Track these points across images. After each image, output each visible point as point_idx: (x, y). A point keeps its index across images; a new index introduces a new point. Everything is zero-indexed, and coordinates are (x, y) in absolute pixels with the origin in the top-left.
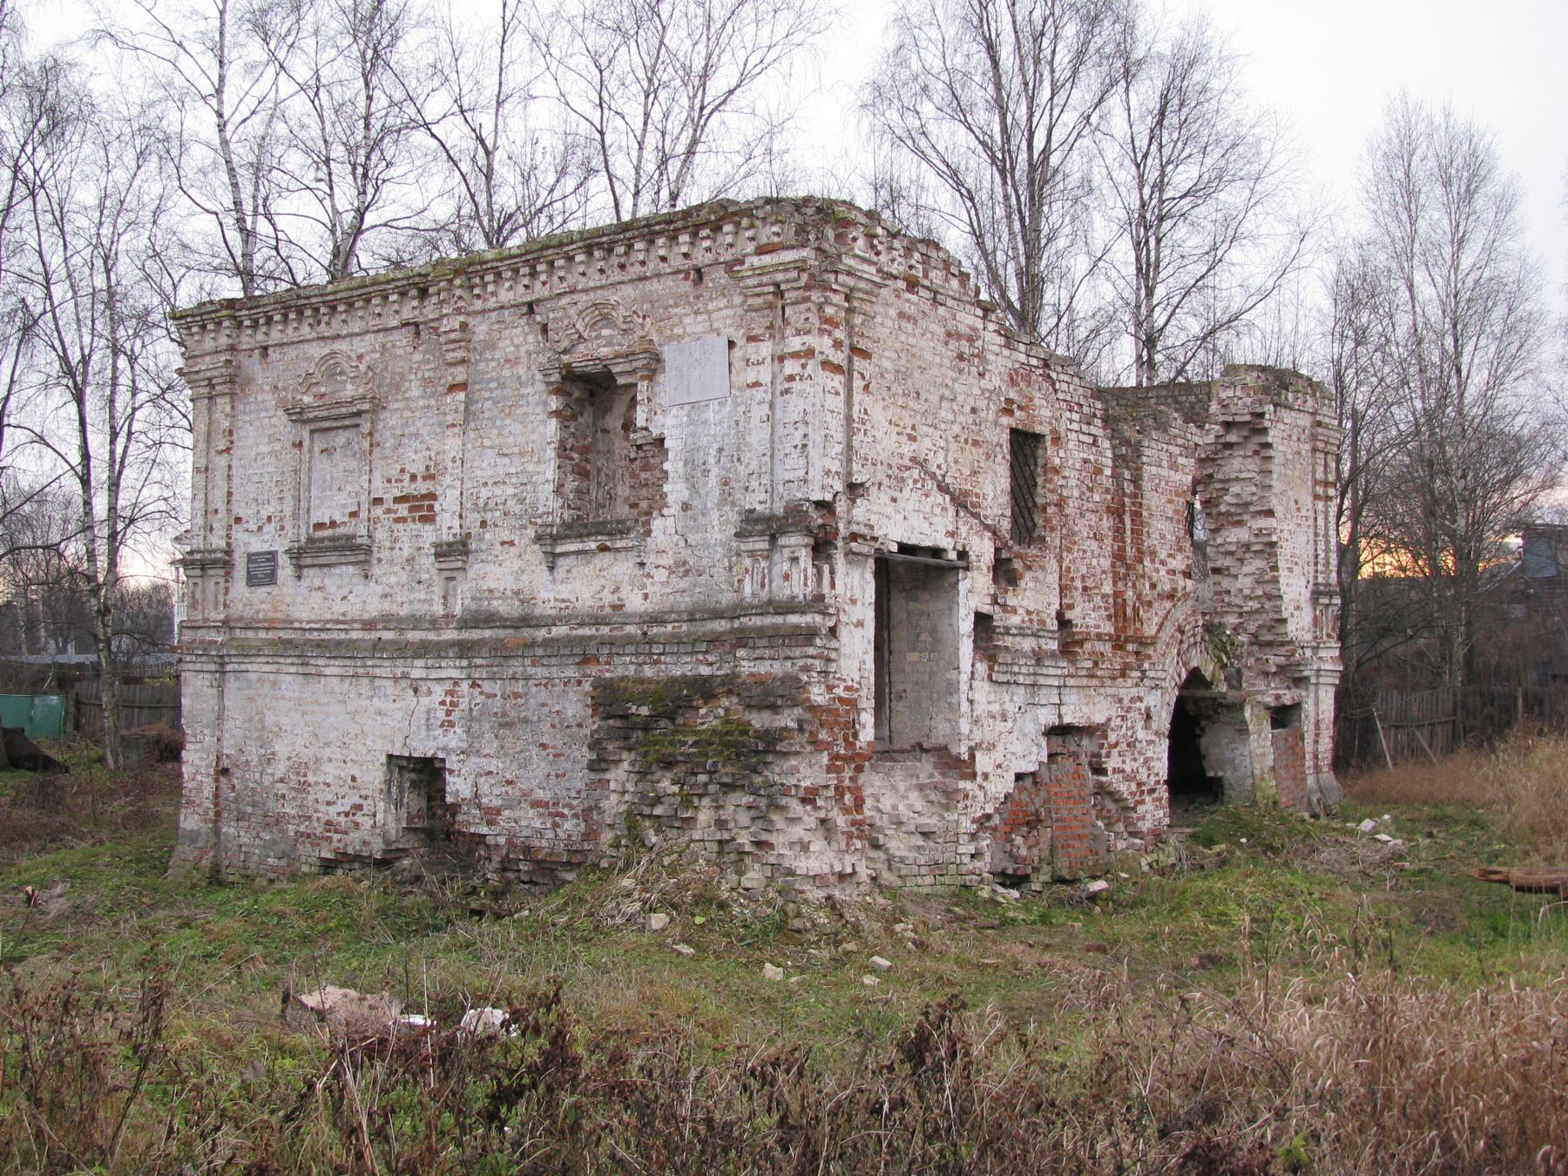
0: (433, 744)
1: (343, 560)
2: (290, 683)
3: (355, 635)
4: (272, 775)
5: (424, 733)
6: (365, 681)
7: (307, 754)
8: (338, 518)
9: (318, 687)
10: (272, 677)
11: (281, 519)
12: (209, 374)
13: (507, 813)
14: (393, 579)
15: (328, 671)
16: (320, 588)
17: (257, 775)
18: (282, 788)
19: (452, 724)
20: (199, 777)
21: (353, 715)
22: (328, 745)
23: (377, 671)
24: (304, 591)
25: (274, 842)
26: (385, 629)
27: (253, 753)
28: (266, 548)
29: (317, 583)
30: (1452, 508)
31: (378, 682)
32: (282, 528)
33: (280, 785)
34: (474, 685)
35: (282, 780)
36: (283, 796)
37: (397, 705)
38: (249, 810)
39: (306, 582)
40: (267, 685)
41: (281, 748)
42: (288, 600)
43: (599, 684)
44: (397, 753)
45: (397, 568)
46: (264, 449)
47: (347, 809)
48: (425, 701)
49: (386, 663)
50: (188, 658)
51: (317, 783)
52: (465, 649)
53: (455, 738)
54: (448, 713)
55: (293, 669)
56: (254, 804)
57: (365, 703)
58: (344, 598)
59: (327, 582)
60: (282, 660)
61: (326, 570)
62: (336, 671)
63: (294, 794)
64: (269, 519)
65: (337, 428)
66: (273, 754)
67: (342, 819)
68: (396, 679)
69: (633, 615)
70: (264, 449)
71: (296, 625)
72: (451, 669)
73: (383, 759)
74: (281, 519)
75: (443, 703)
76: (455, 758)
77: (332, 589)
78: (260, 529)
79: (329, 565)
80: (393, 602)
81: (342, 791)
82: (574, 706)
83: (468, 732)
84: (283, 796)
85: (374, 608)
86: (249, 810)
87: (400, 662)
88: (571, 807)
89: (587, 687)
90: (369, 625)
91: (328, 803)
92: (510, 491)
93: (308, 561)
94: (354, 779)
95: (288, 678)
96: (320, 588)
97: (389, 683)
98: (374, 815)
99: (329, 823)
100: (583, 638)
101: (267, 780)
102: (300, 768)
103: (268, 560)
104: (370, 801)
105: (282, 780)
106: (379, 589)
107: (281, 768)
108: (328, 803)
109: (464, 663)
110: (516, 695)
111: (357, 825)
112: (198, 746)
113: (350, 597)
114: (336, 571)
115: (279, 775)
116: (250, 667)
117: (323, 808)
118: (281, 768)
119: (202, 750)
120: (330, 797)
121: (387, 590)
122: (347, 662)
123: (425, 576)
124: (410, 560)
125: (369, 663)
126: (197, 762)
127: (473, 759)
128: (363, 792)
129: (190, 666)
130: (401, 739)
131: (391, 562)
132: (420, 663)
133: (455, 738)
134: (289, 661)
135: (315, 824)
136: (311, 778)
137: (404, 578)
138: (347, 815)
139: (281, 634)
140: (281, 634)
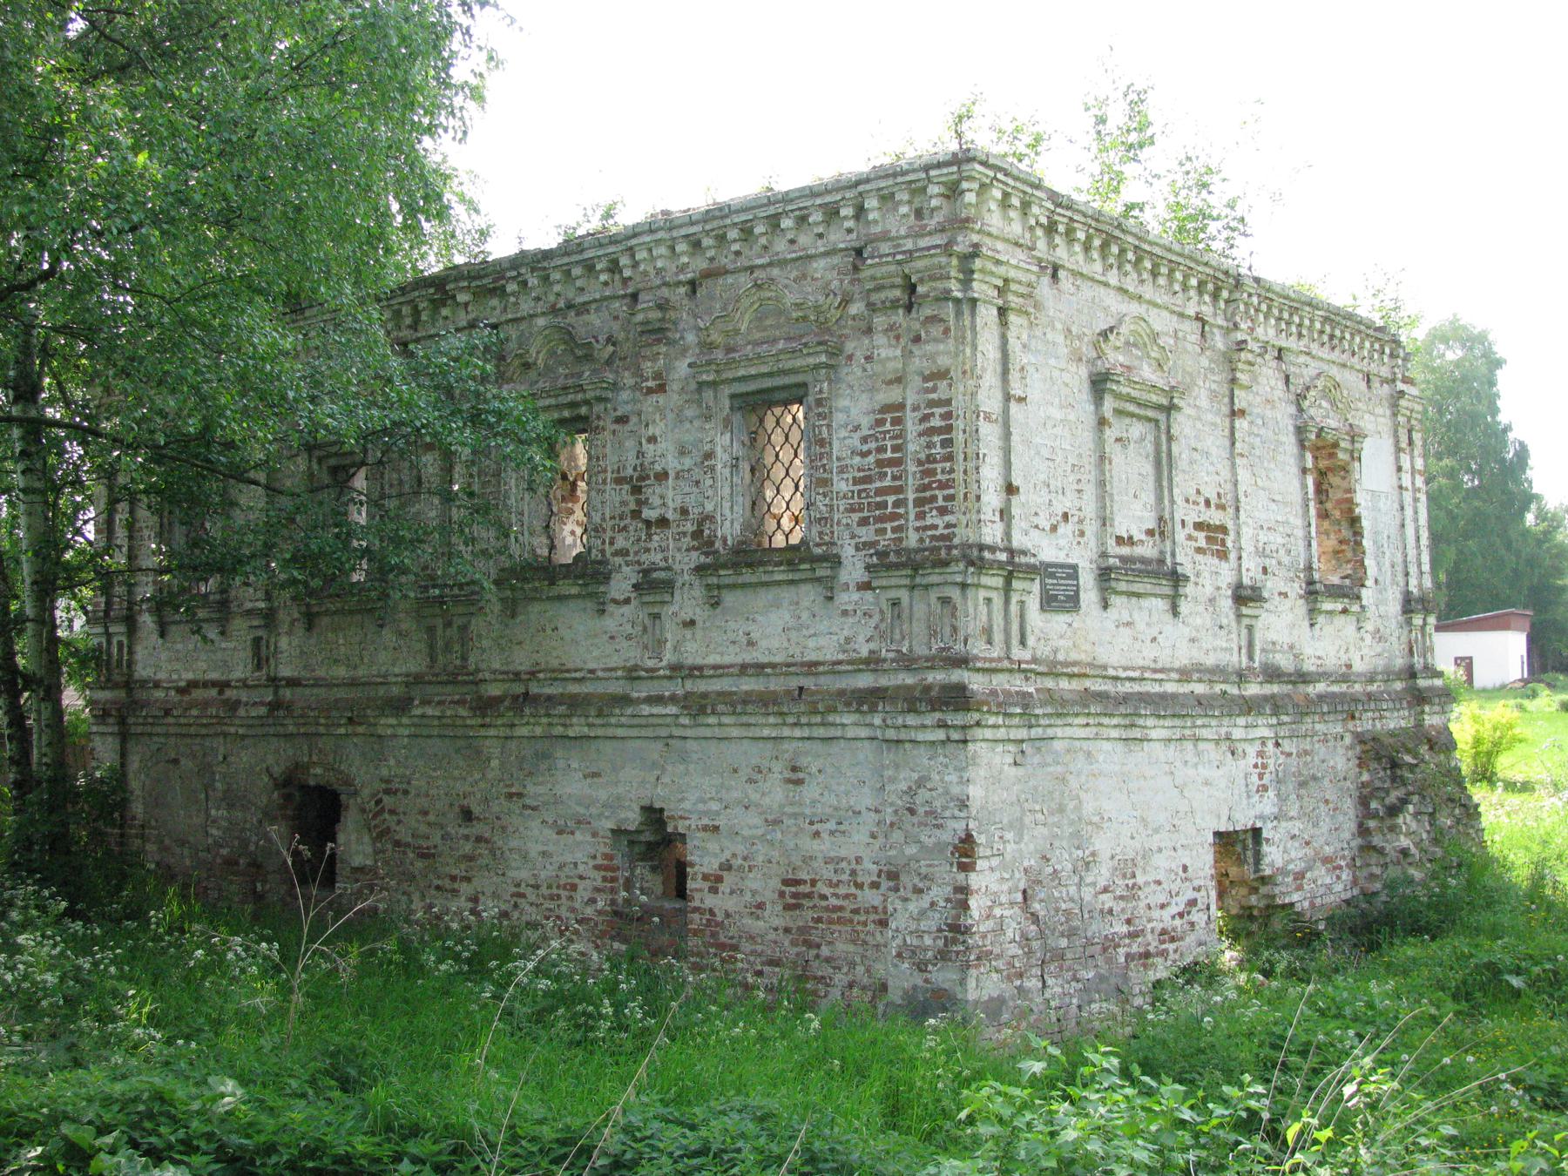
0: (1252, 813)
1: (1157, 590)
2: (1109, 754)
3: (1170, 688)
4: (1094, 884)
5: (1245, 802)
6: (1189, 745)
7: (1130, 848)
8: (1138, 535)
9: (1140, 755)
10: (1085, 745)
11: (1081, 521)
12: (1012, 274)
13: (1308, 875)
14: (1199, 621)
15: (1154, 734)
16: (1128, 624)
17: (1073, 890)
18: (1107, 901)
19: (1265, 788)
20: (997, 912)
21: (1180, 788)
22: (1156, 831)
23: (1205, 733)
24: (1111, 626)
25: (1101, 978)
26: (1200, 681)
27: (1063, 861)
28: (1061, 558)
29: (1126, 618)
30: (487, 349)
31: (1201, 745)
32: (1082, 534)
33: (1102, 897)
34: (1277, 744)
35: (1105, 890)
36: (1111, 911)
37: (1221, 772)
38: (1064, 943)
39: (1113, 613)
40: (1081, 756)
41: (1102, 844)
42: (1092, 637)
43: (1360, 739)
44: (1222, 829)
45: (1201, 608)
46: (1057, 414)
47: (1181, 908)
48: (1242, 763)
49: (1214, 722)
50: (992, 720)
51: (1147, 883)
52: (1275, 705)
53: (1268, 804)
54: (1261, 776)
55: (1114, 733)
56: (1071, 933)
57: (1191, 772)
58: (1154, 640)
59: (1136, 616)
60: (1106, 721)
61: (1134, 600)
62: (1163, 733)
63: (1122, 904)
64: (1065, 516)
65: (1132, 415)
66: (1093, 854)
67: (1178, 922)
68: (1217, 742)
69: (1359, 675)
70: (1057, 414)
71: (1111, 672)
72: (1264, 728)
73: (1211, 839)
74: (1081, 521)
75: (1256, 766)
76: (1270, 825)
77: (1141, 626)
78: (1054, 528)
79: (1138, 595)
80: (1200, 648)
81: (1174, 888)
82: (1340, 760)
83: (1278, 795)
84: (1111, 911)
85: (1185, 656)
86: (1064, 943)
87: (1226, 721)
88: (1343, 857)
89: (1348, 740)
90: (1185, 675)
91: (1163, 906)
92: (1280, 540)
93: (1122, 586)
94: (1185, 868)
95: (1106, 746)
96: (1128, 624)
97: (1211, 746)
98: (1208, 908)
99: (1164, 932)
100: (1334, 695)
101: (1087, 894)
102: (1127, 868)
103: (1069, 577)
104: (1203, 893)
105: (1105, 890)
106: (1186, 631)
107: (1102, 874)
108: (1163, 906)
109: (1274, 721)
110: (1306, 753)
111: (1192, 924)
112: (995, 862)
113: (1160, 638)
114: (1145, 603)
115: (1102, 883)
116: (1059, 732)
117: (1156, 914)
118: (1102, 874)
119: (1004, 866)
120: (1162, 899)
121: (1194, 634)
122: (1177, 722)
123: (1225, 622)
124: (1212, 600)
125: (1199, 722)
126: (994, 887)
127: (1284, 824)
128: (1196, 883)
129: (988, 733)
130: (1226, 812)
131: (1195, 599)
132: (1241, 721)
133: (1268, 804)
134: (1115, 721)
135: (1149, 937)
136: (1140, 880)
137: (1209, 623)
138: (1181, 915)
139: (1088, 683)
140: (1088, 683)
